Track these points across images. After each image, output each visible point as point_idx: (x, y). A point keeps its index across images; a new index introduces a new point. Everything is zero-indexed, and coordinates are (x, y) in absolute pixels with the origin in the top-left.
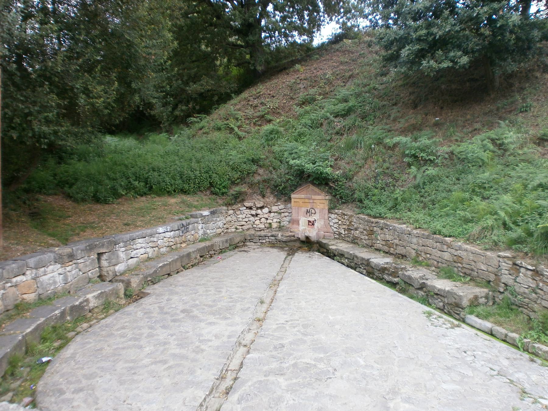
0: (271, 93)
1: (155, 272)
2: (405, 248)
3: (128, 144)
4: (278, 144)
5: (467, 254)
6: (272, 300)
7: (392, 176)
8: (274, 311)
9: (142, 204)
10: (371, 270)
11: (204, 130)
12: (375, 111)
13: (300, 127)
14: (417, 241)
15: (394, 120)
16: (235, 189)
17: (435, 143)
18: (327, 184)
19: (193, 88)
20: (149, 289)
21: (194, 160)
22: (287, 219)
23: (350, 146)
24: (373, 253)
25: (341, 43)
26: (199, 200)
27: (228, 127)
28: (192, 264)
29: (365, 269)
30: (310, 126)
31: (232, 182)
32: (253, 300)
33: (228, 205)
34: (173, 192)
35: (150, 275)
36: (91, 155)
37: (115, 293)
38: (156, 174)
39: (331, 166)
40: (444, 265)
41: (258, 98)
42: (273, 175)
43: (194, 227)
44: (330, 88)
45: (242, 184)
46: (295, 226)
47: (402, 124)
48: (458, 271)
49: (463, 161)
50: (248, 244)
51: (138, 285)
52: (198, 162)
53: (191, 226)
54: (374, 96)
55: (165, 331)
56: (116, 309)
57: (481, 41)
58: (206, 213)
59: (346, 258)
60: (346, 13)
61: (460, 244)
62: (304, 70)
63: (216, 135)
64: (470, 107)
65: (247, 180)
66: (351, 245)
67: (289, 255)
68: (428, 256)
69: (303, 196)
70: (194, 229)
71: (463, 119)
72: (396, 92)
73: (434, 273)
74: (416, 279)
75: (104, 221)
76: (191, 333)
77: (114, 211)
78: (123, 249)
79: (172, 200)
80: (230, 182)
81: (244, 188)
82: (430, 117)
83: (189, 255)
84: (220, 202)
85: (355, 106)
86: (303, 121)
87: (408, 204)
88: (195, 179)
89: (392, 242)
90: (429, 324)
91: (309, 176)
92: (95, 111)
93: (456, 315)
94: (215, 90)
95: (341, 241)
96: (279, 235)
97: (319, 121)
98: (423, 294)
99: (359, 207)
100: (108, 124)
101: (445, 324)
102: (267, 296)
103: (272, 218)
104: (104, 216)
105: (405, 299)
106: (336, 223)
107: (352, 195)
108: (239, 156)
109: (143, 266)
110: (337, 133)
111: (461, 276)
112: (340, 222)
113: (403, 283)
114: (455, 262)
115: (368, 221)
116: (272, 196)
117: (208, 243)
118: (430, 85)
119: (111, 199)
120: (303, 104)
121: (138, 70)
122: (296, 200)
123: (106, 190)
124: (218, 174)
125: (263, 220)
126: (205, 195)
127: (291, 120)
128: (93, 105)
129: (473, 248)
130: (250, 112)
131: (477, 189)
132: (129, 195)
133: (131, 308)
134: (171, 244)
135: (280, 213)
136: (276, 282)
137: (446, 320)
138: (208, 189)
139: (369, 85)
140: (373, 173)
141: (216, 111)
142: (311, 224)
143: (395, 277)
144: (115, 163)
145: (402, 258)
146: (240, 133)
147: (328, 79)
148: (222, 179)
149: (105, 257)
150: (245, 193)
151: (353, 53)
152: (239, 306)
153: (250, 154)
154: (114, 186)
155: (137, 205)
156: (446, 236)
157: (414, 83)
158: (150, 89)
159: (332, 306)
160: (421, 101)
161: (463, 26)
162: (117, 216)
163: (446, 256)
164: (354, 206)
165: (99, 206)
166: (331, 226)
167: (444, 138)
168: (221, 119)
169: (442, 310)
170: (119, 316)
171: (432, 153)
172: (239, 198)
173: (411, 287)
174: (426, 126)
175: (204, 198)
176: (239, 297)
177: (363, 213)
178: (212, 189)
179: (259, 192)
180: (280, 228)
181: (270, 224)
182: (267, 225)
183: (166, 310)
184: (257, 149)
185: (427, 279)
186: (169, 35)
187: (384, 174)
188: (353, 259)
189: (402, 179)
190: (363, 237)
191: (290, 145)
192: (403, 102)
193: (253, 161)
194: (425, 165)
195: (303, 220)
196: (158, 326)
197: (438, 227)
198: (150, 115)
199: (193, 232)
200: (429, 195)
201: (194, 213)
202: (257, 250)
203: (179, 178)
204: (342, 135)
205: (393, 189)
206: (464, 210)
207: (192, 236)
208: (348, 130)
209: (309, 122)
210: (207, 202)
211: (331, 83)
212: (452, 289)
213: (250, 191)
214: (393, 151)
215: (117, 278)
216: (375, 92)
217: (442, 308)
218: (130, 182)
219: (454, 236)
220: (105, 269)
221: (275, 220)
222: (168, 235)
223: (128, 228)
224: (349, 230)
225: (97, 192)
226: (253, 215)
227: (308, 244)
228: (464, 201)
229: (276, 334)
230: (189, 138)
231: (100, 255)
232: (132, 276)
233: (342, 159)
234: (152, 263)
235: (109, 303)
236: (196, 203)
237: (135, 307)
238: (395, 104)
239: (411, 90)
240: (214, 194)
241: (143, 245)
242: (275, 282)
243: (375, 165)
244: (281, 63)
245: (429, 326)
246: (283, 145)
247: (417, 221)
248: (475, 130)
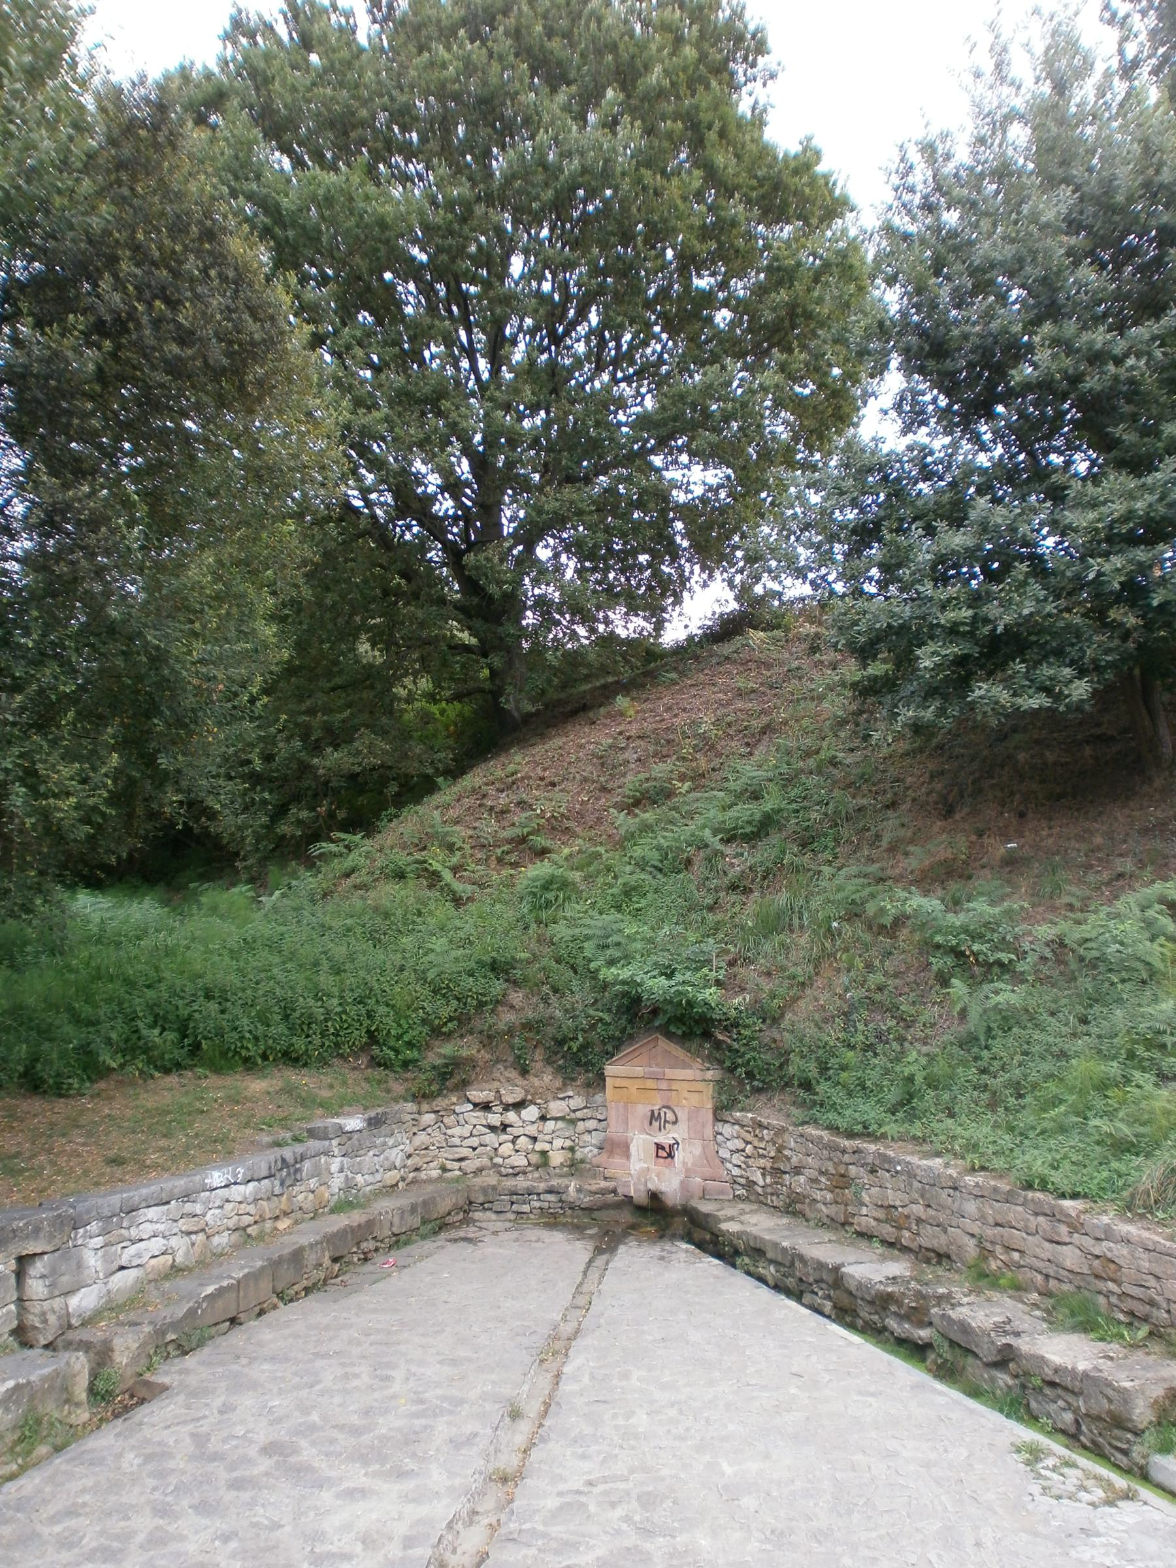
0: (544, 775)
1: (192, 1312)
2: (945, 1232)
3: (138, 916)
4: (565, 918)
5: (1132, 1253)
6: (547, 1405)
8: (551, 1445)
9: (167, 1098)
10: (846, 1301)
11: (354, 879)
12: (836, 825)
13: (628, 869)
14: (979, 1209)
15: (892, 849)
16: (442, 1051)
17: (1008, 913)
18: (707, 1035)
19: (334, 760)
20: (167, 1373)
21: (325, 965)
22: (595, 1138)
23: (773, 924)
24: (851, 1244)
25: (738, 641)
26: (336, 1083)
27: (426, 870)
28: (305, 1283)
29: (828, 1297)
30: (655, 867)
31: (433, 1030)
32: (488, 1407)
33: (421, 1097)
34: (259, 1061)
35: (174, 1325)
36: (29, 949)
37: (61, 1387)
38: (213, 1006)
39: (718, 983)
40: (1066, 1287)
41: (509, 787)
42: (551, 1009)
43: (317, 1166)
44: (710, 761)
45: (462, 1036)
46: (617, 1160)
47: (916, 860)
48: (1110, 1304)
49: (1095, 967)
50: (477, 1215)
51: (134, 1360)
52: (337, 971)
53: (307, 1165)
54: (835, 782)
55: (207, 1522)
56: (59, 1441)
57: (1116, 642)
58: (354, 1123)
59: (771, 1261)
60: (751, 559)
61: (1105, 1219)
62: (637, 712)
63: (388, 893)
64: (1100, 813)
65: (477, 1024)
66: (785, 1221)
67: (598, 1251)
68: (1016, 1255)
69: (639, 1070)
70: (316, 1173)
71: (1084, 847)
72: (893, 772)
73: (1038, 1313)
74: (983, 1332)
75: (49, 1151)
76: (288, 1529)
77: (83, 1121)
78: (98, 1241)
79: (256, 1086)
80: (426, 1029)
81: (467, 1047)
82: (992, 841)
83: (297, 1255)
84: (398, 1088)
85: (780, 810)
86: (638, 852)
87: (946, 1096)
88: (326, 1020)
89: (906, 1211)
90: (1036, 1489)
91: (655, 1012)
92: (52, 830)
93: (1119, 1456)
94: (390, 768)
95: (755, 1207)
96: (571, 1189)
97: (683, 851)
98: (1010, 1382)
99: (803, 1104)
100: (86, 864)
101: (1086, 1490)
102: (530, 1391)
103: (548, 1138)
104: (50, 1136)
105: (955, 1402)
106: (738, 1151)
107: (781, 1067)
108: (454, 954)
109: (154, 1296)
110: (733, 887)
111: (1119, 1322)
112: (749, 1148)
113: (946, 1344)
114: (1097, 1277)
116: (550, 1069)
117: (356, 1217)
118: (985, 753)
119: (75, 1082)
120: (635, 803)
121: (180, 723)
122: (618, 1083)
123: (63, 1055)
124: (393, 1006)
125: (523, 1142)
126: (355, 1069)
127: (601, 849)
128: (45, 815)
129: (1146, 1234)
130: (489, 827)
131: (1140, 1051)
132: (130, 1069)
133: (105, 1440)
134: (247, 1220)
135: (573, 1122)
136: (558, 1345)
137: (1088, 1475)
138: (362, 1049)
139: (817, 752)
140: (839, 1002)
141: (392, 825)
142: (665, 1152)
143: (922, 1324)
144: (98, 976)
145: (939, 1263)
146: (458, 886)
147: (704, 737)
148: (403, 1022)
149: (38, 1267)
150: (471, 1062)
151: (769, 666)
152: (442, 1429)
153: (486, 948)
154: (89, 1044)
155: (149, 1101)
156: (1063, 1196)
157: (940, 747)
158: (209, 769)
159: (731, 1427)
160: (962, 796)
161: (1062, 603)
162: (90, 1134)
163: (1070, 1257)
164: (788, 1099)
165: (36, 1104)
166: (723, 1160)
167: (1035, 899)
168: (404, 847)
169: (1072, 1436)
170: (63, 1467)
171: (1003, 945)
172: (451, 1078)
173: (970, 1360)
174: (983, 867)
175: (351, 1076)
176: (444, 1398)
177: (816, 1121)
178: (376, 1051)
179: (511, 1059)
180: (575, 1166)
181: (544, 1153)
182: (534, 1158)
183: (213, 1445)
184: (506, 933)
185: (1017, 1334)
186: (268, 632)
187: (871, 1004)
188: (792, 1264)
189: (922, 1019)
190: (818, 1195)
191: (600, 922)
192: (914, 800)
193: (493, 969)
194: (986, 978)
195: (641, 1143)
196: (185, 1503)
197: (1039, 1167)
198: (206, 833)
199: (313, 1183)
200: (1003, 1068)
201: (318, 1124)
202: (503, 1236)
203: (277, 1018)
204: (747, 891)
205: (898, 1048)
206: (1110, 1114)
207: (311, 1196)
208: (764, 878)
209: (654, 857)
210: (357, 1089)
211: (712, 747)
212: (1096, 1369)
213: (485, 1055)
214: (893, 937)
215: (71, 1335)
216: (835, 772)
217: (1072, 1430)
218: (136, 1031)
219: (1085, 1196)
220: (36, 1308)
221: (558, 1143)
222: (238, 1192)
223: (118, 1171)
224: (777, 1172)
225: (37, 1060)
226: (493, 1128)
227: (658, 1218)
228: (1107, 1087)
229: (556, 1530)
230: (313, 901)
231: (24, 1261)
232: (120, 1330)
233: (748, 961)
234: (183, 1284)
235: (38, 1422)
236: (326, 1093)
237: (117, 1435)
238: (892, 805)
239: (932, 766)
240: (379, 1065)
241: (161, 1227)
242: (558, 1345)
243: (844, 979)
244: (574, 691)
245: (1038, 1497)
246: (581, 921)
247: (975, 1147)
248: (1121, 876)
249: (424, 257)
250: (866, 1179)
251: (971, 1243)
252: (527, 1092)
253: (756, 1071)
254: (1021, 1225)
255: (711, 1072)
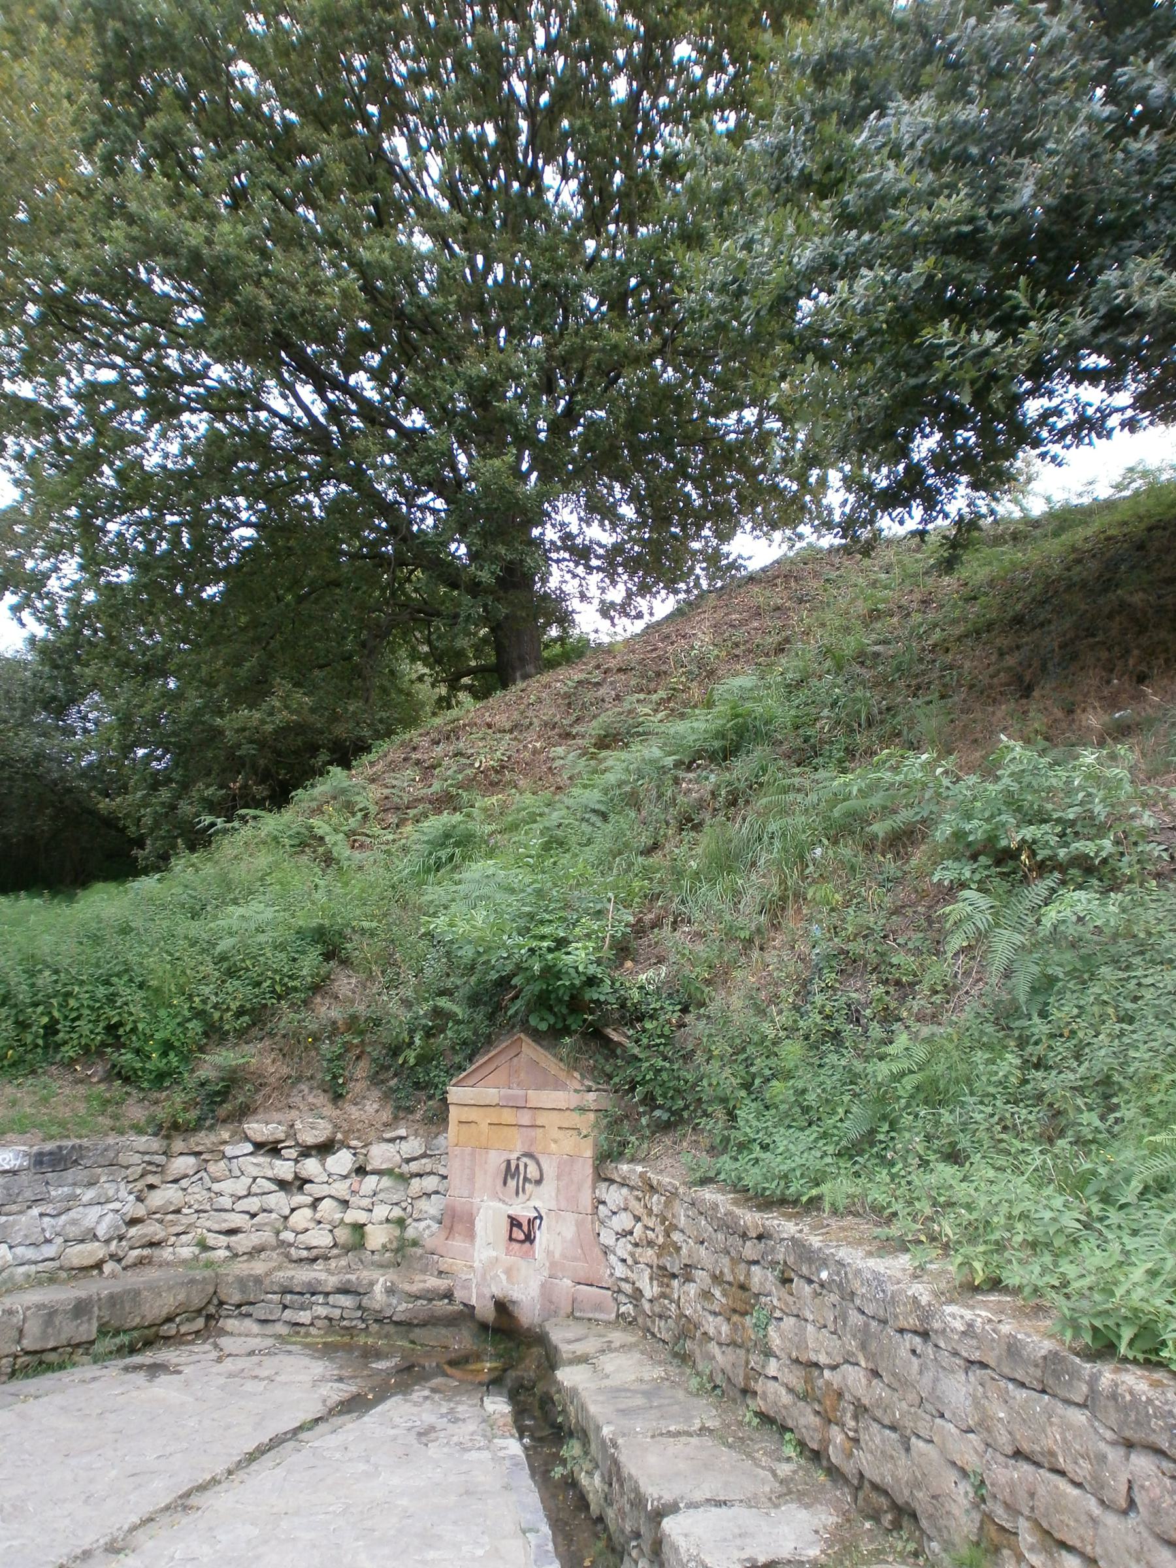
7: (880, 968)
23: (727, 861)
24: (741, 1444)
33: (172, 1129)
46: (458, 1243)
50: (231, 1324)
69: (491, 1093)
80: (195, 1026)
84: (136, 1112)
96: (378, 1288)
103: (366, 1202)
115: (729, 1226)
116: (376, 1093)
135: (404, 1179)
142: (522, 1232)
166: (606, 1251)
172: (226, 1102)
180: (403, 1251)
181: (359, 1228)
182: (343, 1235)
195: (491, 1214)
197: (1136, 1289)
221: (381, 1212)
226: (283, 1185)
249: (602, 414)
250: (776, 1297)
251: (962, 1493)
252: (337, 1127)
253: (658, 1091)
254: (1083, 1469)
255: (592, 1096)
